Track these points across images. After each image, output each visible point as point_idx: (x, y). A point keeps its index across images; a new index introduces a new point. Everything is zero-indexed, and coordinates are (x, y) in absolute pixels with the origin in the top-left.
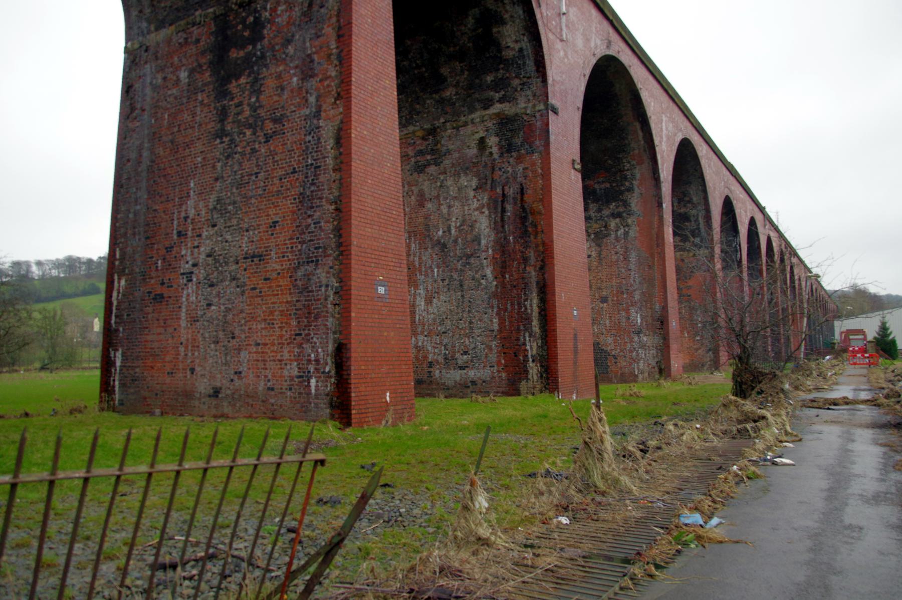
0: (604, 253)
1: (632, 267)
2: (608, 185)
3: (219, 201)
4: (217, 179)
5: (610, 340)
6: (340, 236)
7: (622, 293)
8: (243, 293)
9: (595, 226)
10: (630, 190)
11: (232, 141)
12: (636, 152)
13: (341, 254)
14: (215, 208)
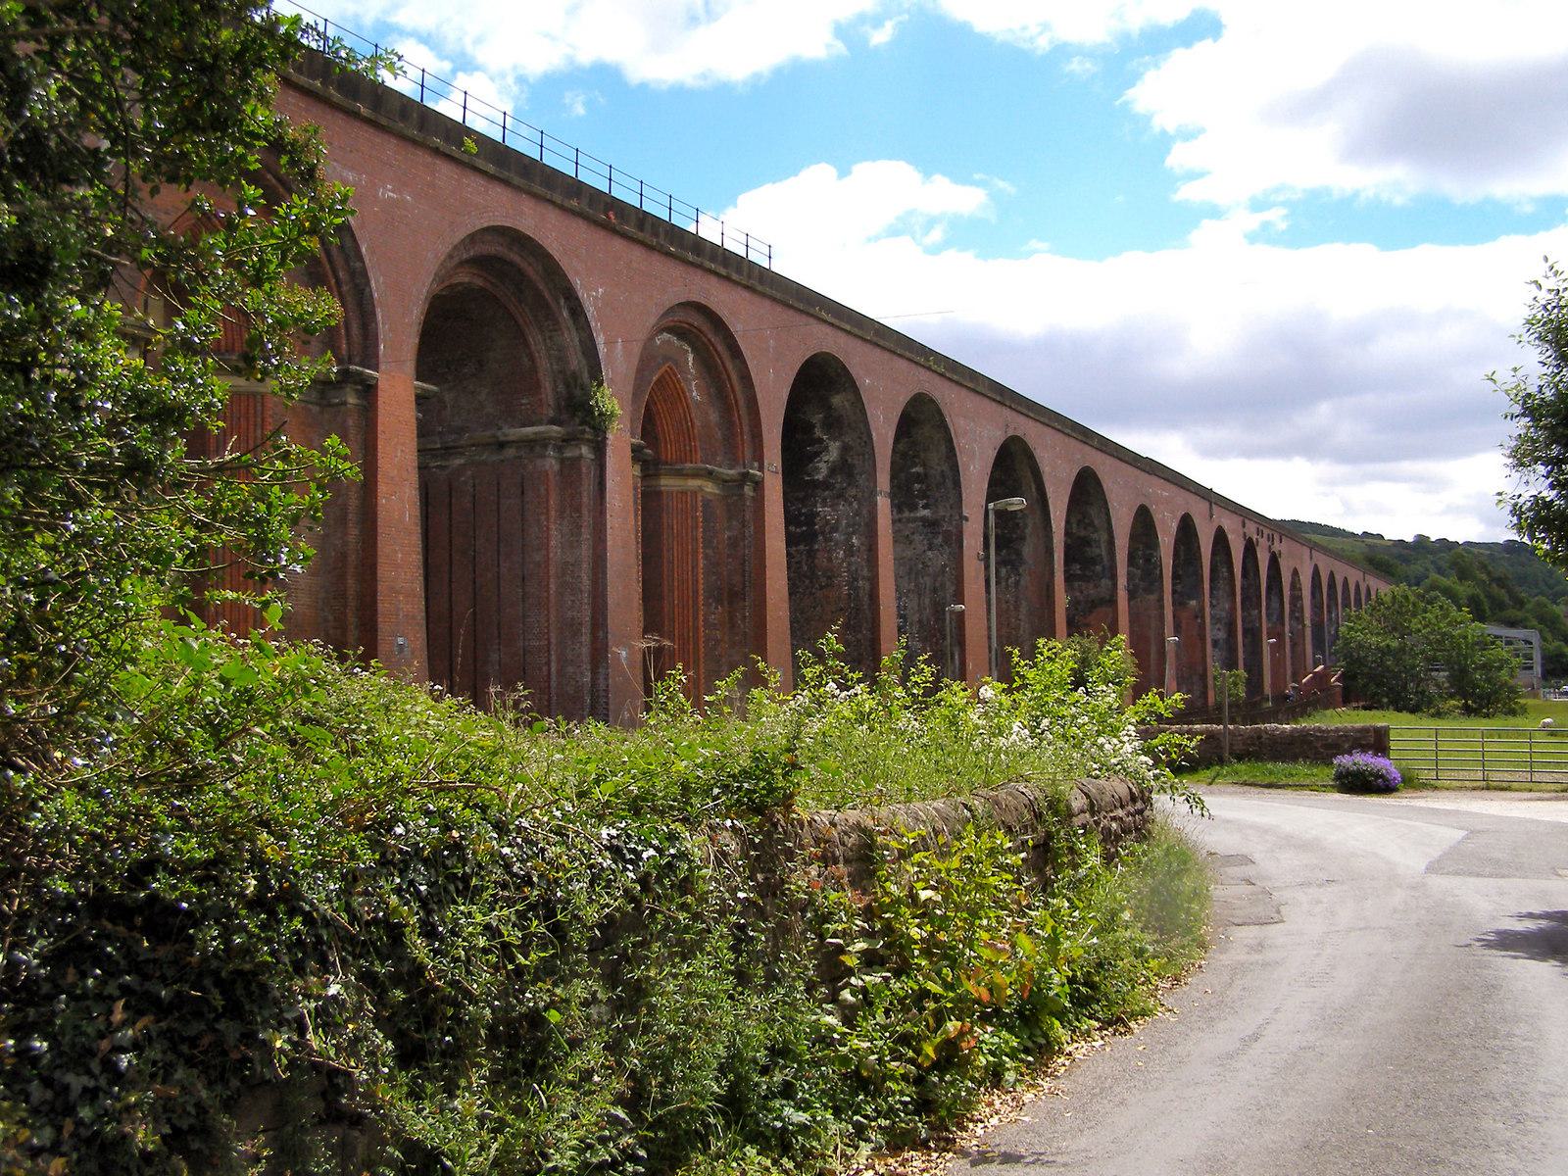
10: (1023, 538)
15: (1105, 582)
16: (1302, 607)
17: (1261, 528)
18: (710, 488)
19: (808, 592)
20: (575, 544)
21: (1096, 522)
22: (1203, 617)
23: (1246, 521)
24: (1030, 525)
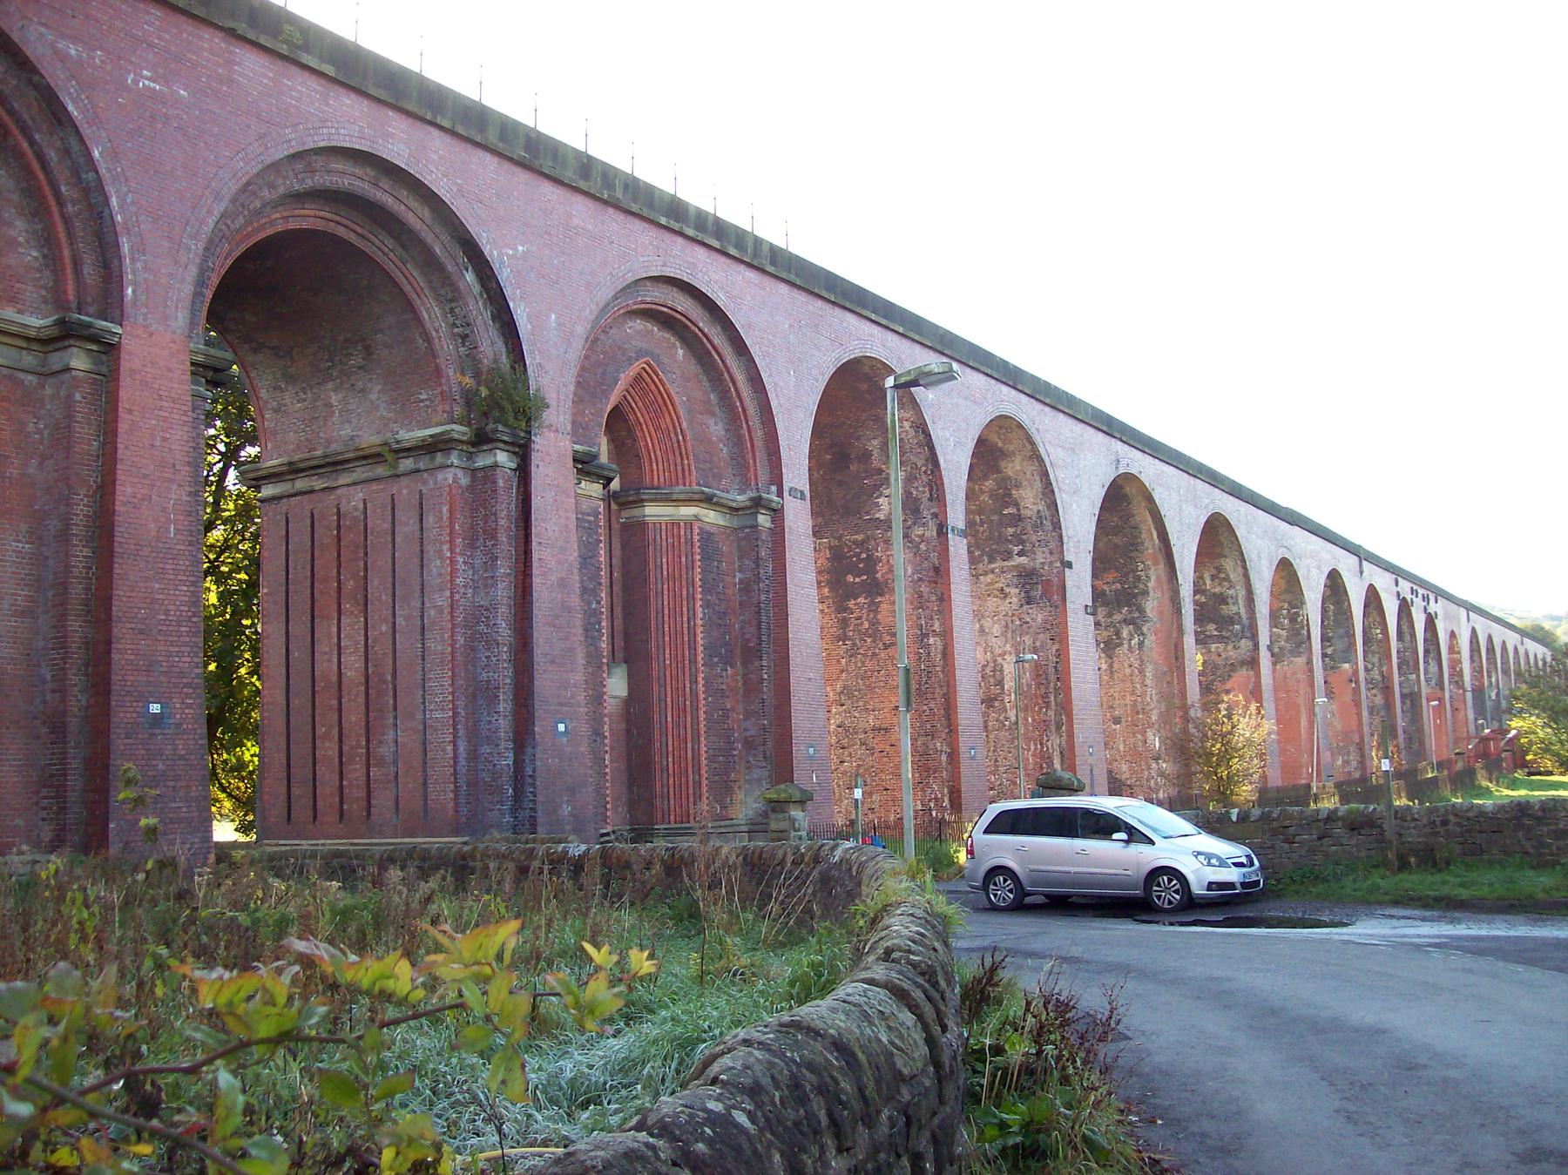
0: (1116, 666)
1: (1148, 682)
2: (1118, 586)
3: (845, 687)
4: (842, 671)
5: (1125, 767)
6: (949, 719)
7: (1138, 713)
8: (873, 754)
9: (1105, 634)
10: (1145, 593)
11: (854, 645)
12: (1151, 551)
13: (951, 731)
14: (842, 692)
15: (1245, 644)
16: (1461, 670)
17: (1415, 587)
18: (711, 517)
19: (870, 653)
20: (490, 582)
21: (1232, 576)
22: (1357, 682)
23: (1399, 579)
24: (1153, 578)
